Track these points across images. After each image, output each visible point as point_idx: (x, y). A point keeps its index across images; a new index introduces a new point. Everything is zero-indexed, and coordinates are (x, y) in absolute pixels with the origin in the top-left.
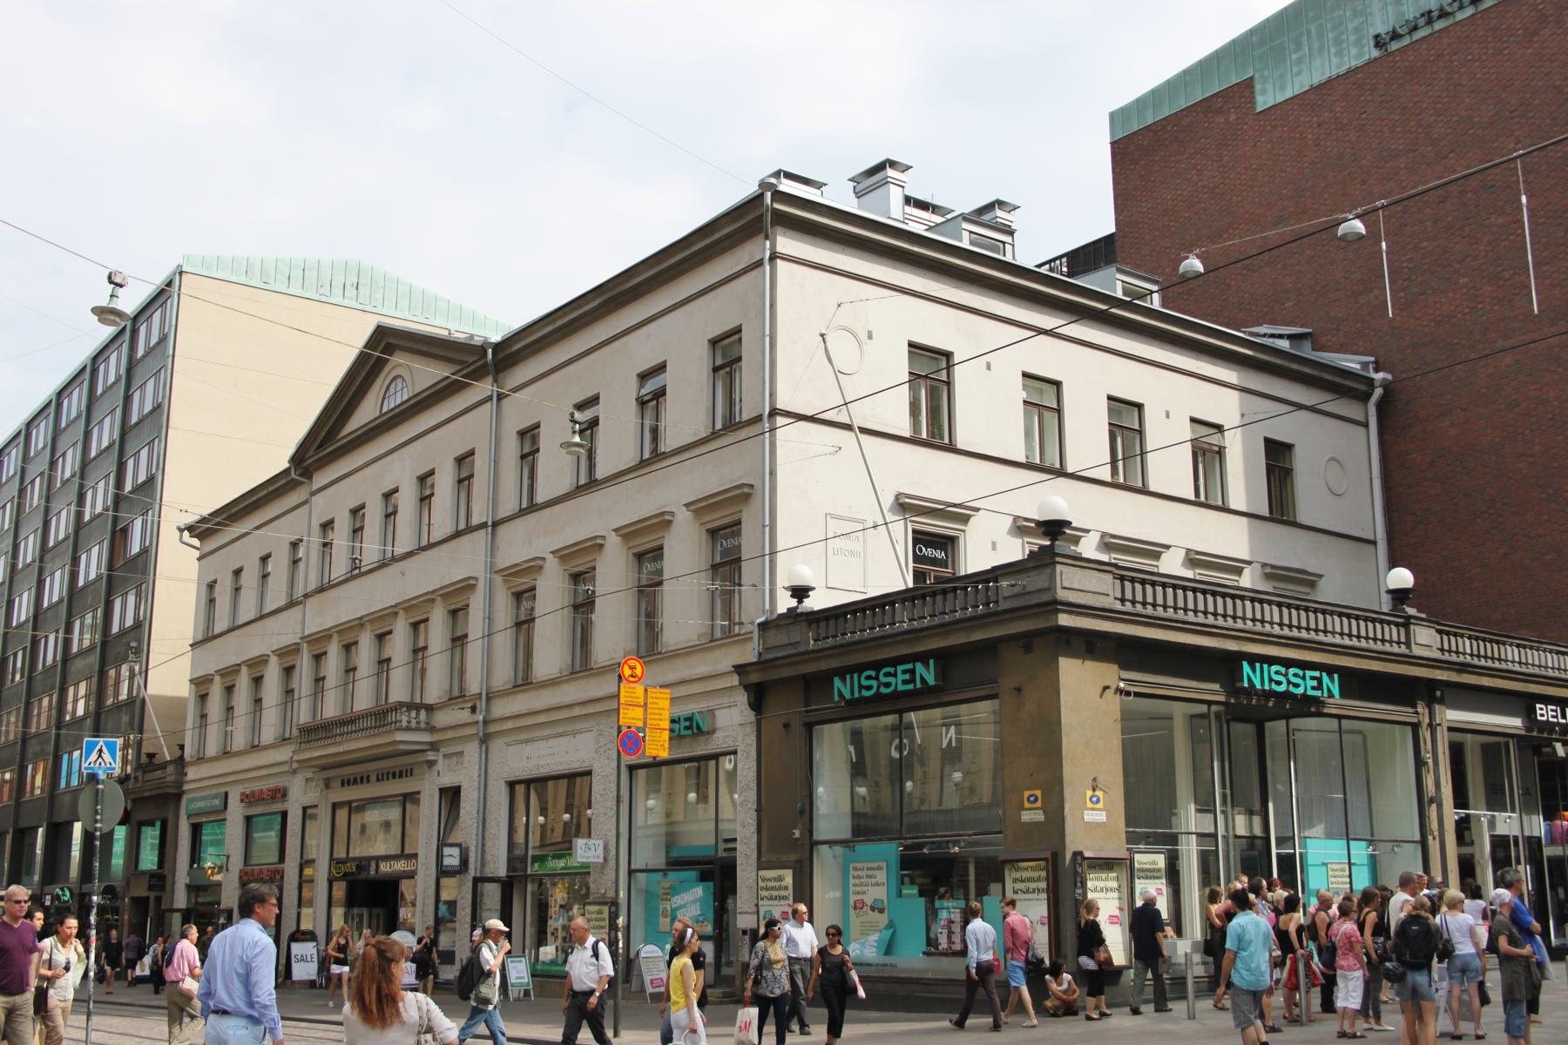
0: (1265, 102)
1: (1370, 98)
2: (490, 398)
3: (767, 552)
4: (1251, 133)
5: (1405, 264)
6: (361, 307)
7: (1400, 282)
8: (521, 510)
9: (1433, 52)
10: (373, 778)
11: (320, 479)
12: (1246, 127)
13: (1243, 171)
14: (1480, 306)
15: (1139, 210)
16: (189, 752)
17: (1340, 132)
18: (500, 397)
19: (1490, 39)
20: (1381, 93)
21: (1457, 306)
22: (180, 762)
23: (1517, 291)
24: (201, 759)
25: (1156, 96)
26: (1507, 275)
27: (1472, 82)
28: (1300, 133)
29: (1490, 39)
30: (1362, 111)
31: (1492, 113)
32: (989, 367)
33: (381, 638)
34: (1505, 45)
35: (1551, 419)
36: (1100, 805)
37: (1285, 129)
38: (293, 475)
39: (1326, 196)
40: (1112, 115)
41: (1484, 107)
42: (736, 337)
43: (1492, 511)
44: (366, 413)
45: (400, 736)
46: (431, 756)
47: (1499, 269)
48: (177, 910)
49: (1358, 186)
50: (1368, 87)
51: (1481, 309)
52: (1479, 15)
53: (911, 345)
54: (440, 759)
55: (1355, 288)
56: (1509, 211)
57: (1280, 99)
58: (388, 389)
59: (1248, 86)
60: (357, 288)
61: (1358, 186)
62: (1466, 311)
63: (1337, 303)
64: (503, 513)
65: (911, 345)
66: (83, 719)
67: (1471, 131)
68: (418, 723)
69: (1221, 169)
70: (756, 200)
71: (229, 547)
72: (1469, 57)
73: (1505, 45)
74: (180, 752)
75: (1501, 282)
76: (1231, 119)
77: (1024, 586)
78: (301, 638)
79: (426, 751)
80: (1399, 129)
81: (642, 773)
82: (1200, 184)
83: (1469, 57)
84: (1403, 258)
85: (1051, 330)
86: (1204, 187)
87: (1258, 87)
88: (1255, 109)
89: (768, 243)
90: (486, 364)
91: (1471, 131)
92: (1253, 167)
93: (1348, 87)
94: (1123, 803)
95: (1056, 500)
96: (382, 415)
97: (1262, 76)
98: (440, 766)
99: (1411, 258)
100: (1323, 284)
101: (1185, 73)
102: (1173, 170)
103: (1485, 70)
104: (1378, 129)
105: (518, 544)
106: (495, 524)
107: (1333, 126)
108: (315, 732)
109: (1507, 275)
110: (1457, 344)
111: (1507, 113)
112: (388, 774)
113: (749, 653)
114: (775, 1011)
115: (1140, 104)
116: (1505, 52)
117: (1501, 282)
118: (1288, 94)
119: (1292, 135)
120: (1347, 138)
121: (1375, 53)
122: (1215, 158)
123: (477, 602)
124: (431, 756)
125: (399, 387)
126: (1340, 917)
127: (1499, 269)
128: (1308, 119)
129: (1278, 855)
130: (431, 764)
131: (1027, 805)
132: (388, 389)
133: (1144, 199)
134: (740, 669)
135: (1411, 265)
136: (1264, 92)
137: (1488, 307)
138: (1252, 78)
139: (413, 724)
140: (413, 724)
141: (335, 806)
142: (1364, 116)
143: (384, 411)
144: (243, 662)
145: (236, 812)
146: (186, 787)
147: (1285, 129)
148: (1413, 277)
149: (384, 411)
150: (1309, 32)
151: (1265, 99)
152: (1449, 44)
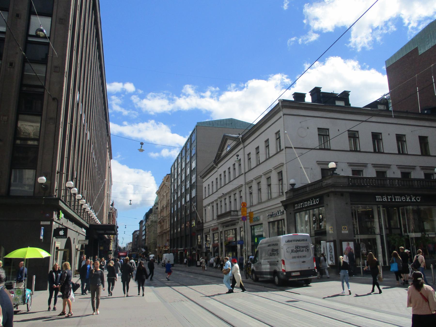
2: (242, 148)
6: (233, 128)
10: (230, 225)
11: (219, 165)
16: (204, 222)
18: (244, 147)
22: (203, 223)
24: (206, 222)
25: (395, 55)
32: (339, 130)
33: (235, 194)
36: (346, 229)
38: (214, 166)
40: (386, 62)
46: (237, 221)
48: (204, 252)
53: (318, 128)
54: (240, 221)
57: (424, 51)
59: (416, 50)
64: (246, 171)
65: (318, 128)
66: (189, 215)
68: (235, 214)
71: (383, 124)
77: (327, 182)
79: (236, 220)
81: (271, 224)
87: (419, 49)
88: (419, 55)
90: (240, 142)
94: (50, 261)
95: (355, 158)
96: (227, 152)
98: (239, 223)
101: (402, 49)
105: (251, 176)
106: (245, 173)
108: (219, 217)
113: (284, 198)
114: (265, 275)
115: (392, 58)
118: (427, 49)
123: (243, 189)
124: (237, 221)
126: (343, 257)
130: (238, 222)
131: (343, 229)
134: (282, 202)
136: (421, 50)
138: (417, 47)
139: (234, 214)
141: (225, 231)
144: (215, 201)
145: (211, 233)
146: (204, 228)
151: (421, 52)
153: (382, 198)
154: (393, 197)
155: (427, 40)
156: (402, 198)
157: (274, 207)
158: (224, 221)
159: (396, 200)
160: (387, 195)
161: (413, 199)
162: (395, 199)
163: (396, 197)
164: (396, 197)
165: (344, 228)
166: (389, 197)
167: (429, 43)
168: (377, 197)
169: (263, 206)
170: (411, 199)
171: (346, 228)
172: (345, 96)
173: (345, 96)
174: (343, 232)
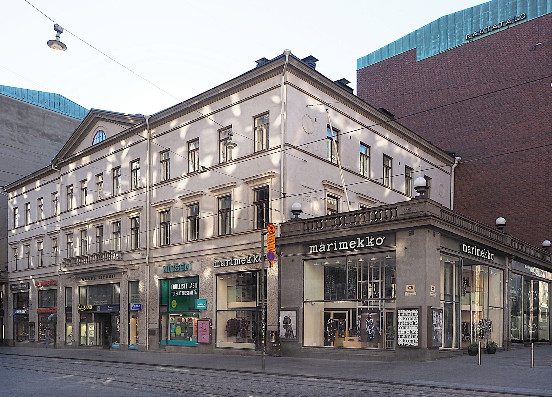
0: (420, 58)
1: (462, 58)
3: (148, 230)
4: (413, 69)
5: (469, 120)
7: (467, 126)
8: (254, 153)
9: (489, 42)
12: (412, 67)
13: (409, 83)
14: (497, 135)
15: (366, 96)
17: (449, 71)
19: (513, 39)
20: (467, 57)
21: (488, 135)
23: (512, 131)
25: (376, 54)
26: (508, 125)
27: (504, 54)
28: (433, 70)
29: (513, 39)
30: (458, 63)
31: (510, 66)
34: (518, 41)
35: (519, 175)
36: (413, 289)
37: (427, 68)
39: (441, 94)
41: (507, 64)
42: (268, 115)
43: (493, 205)
44: (86, 144)
45: (113, 263)
47: (506, 123)
49: (454, 91)
50: (462, 54)
51: (497, 137)
52: (509, 29)
55: (449, 127)
56: (512, 102)
58: (95, 135)
59: (414, 52)
60: (59, 105)
61: (454, 91)
62: (492, 137)
63: (442, 133)
67: (501, 73)
68: (115, 258)
69: (400, 82)
70: (283, 56)
72: (503, 45)
73: (518, 41)
74: (6, 269)
75: (506, 127)
76: (406, 64)
78: (60, 228)
80: (472, 70)
82: (391, 87)
83: (503, 45)
84: (469, 118)
85: (369, 127)
86: (393, 88)
87: (418, 52)
89: (283, 77)
91: (501, 73)
92: (413, 82)
93: (454, 54)
96: (93, 146)
97: (420, 48)
99: (472, 118)
100: (437, 125)
102: (381, 82)
103: (509, 50)
104: (464, 70)
107: (446, 68)
109: (508, 125)
110: (486, 148)
111: (516, 67)
112: (104, 276)
116: (518, 44)
117: (506, 127)
119: (430, 71)
120: (452, 73)
121: (466, 42)
122: (398, 78)
124: (125, 270)
125: (101, 135)
127: (506, 123)
128: (437, 65)
129: (345, 318)
132: (95, 135)
133: (369, 92)
135: (472, 120)
136: (420, 54)
137: (500, 136)
140: (114, 258)
142: (459, 65)
143: (94, 144)
147: (427, 68)
148: (472, 124)
149: (94, 144)
150: (440, 32)
151: (421, 57)
152: (496, 40)
153: (319, 248)
154: (335, 244)
155: (433, 41)
156: (350, 244)
157: (191, 255)
158: (358, 116)
159: (340, 248)
160: (326, 242)
161: (370, 243)
162: (338, 246)
163: (340, 243)
164: (340, 243)
165: (408, 288)
166: (329, 245)
167: (435, 48)
168: (311, 247)
169: (44, 271)
170: (365, 242)
171: (412, 288)
172: (311, 61)
173: (311, 61)
174: (407, 294)
